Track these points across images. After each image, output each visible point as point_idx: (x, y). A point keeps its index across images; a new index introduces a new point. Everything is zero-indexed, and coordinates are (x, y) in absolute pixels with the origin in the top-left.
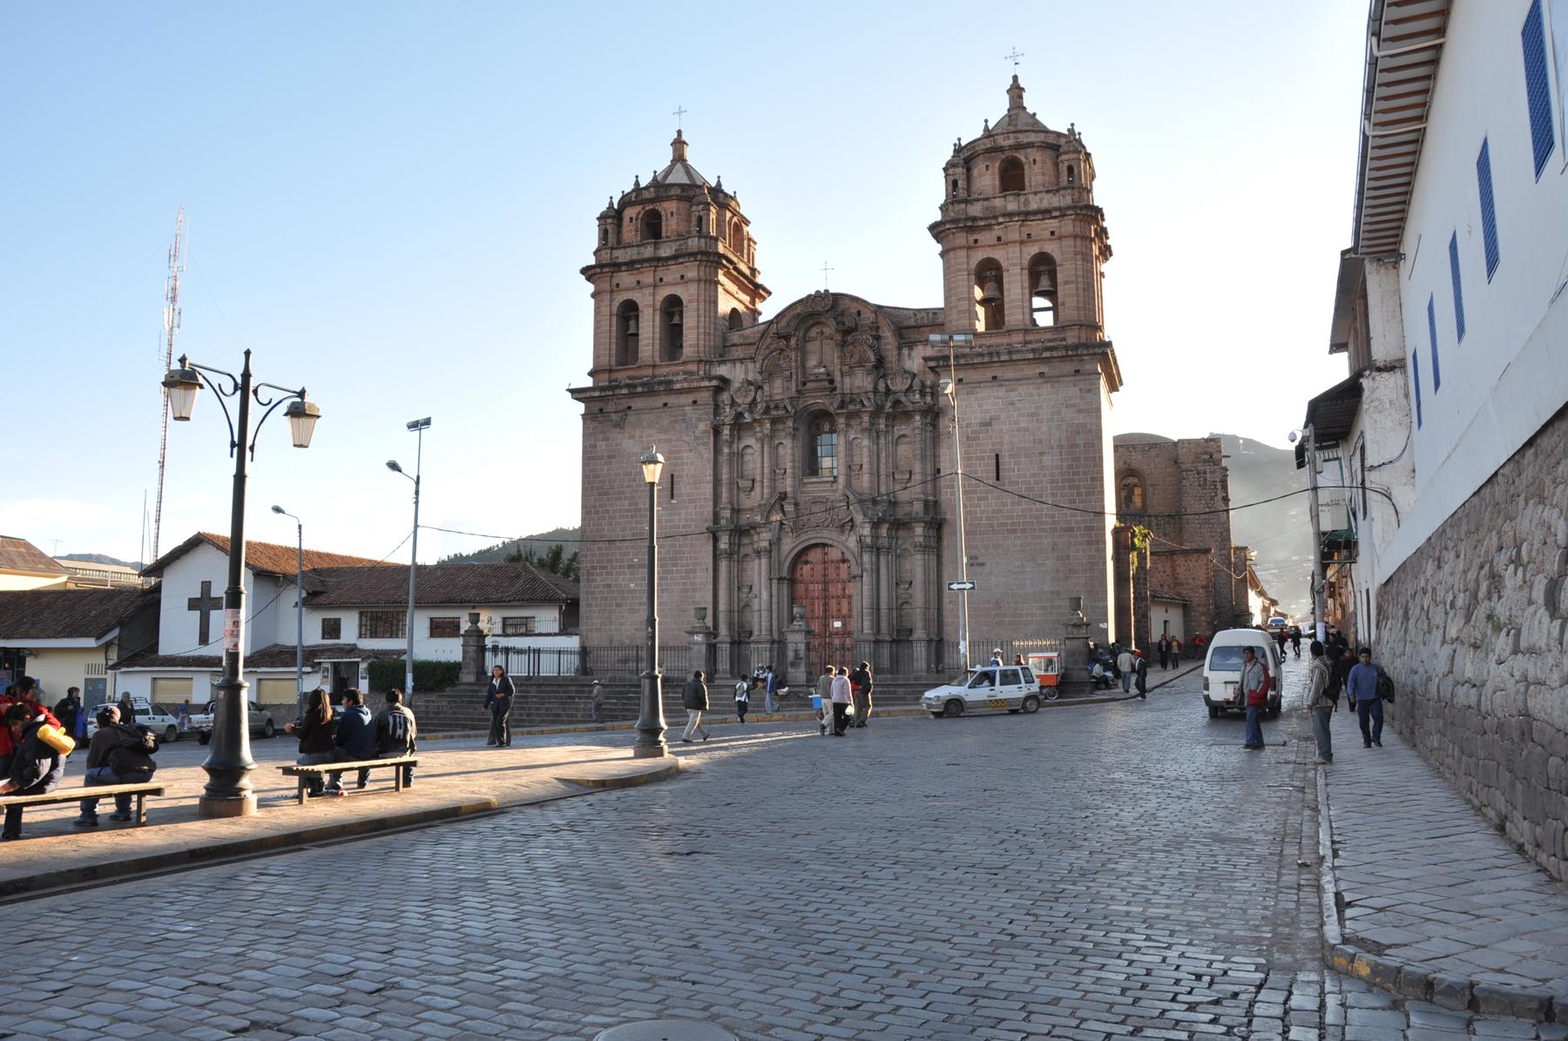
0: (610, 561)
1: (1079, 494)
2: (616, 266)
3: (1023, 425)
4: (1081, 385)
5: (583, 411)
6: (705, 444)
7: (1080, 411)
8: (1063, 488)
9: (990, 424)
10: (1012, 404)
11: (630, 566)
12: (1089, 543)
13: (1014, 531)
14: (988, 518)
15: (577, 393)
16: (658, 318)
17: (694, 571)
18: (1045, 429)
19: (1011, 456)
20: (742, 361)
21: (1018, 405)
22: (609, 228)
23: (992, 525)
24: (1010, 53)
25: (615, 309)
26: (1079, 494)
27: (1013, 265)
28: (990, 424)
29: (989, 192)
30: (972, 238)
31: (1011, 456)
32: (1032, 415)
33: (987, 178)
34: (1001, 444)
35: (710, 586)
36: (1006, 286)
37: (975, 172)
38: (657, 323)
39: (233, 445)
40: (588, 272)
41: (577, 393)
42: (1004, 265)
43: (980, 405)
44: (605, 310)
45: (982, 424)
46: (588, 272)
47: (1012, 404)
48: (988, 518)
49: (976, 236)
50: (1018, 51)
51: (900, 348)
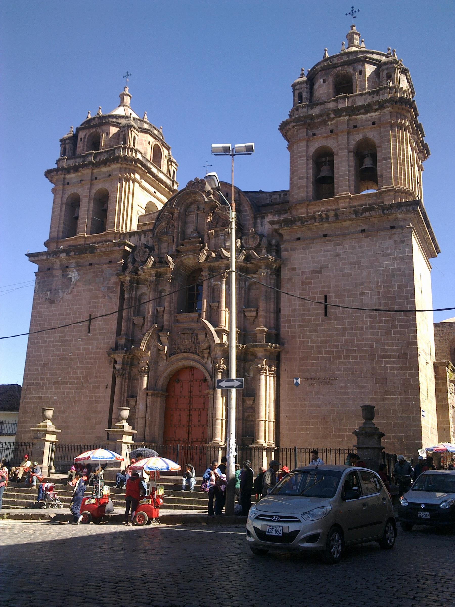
0: (42, 379)
1: (394, 327)
2: (68, 170)
3: (346, 271)
4: (396, 237)
5: (37, 270)
6: (115, 292)
7: (395, 259)
8: (381, 322)
9: (320, 272)
10: (338, 255)
11: (55, 383)
12: (403, 368)
13: (340, 358)
14: (318, 347)
15: (32, 256)
16: (92, 205)
17: (98, 387)
18: (365, 274)
19: (337, 296)
20: (266, 308)
21: (343, 256)
22: (67, 146)
23: (320, 353)
24: (350, 10)
25: (65, 200)
26: (394, 327)
27: (342, 149)
28: (320, 272)
29: (324, 99)
30: (311, 133)
31: (337, 296)
32: (353, 263)
33: (323, 88)
34: (329, 287)
35: (109, 399)
36: (335, 166)
37: (316, 86)
38: (91, 208)
39: (191, 421)
40: (48, 174)
41: (32, 256)
42: (335, 150)
43: (313, 258)
44: (59, 200)
45: (314, 272)
46: (48, 174)
47: (338, 255)
48: (318, 347)
49: (314, 131)
50: (356, 9)
51: (255, 219)
